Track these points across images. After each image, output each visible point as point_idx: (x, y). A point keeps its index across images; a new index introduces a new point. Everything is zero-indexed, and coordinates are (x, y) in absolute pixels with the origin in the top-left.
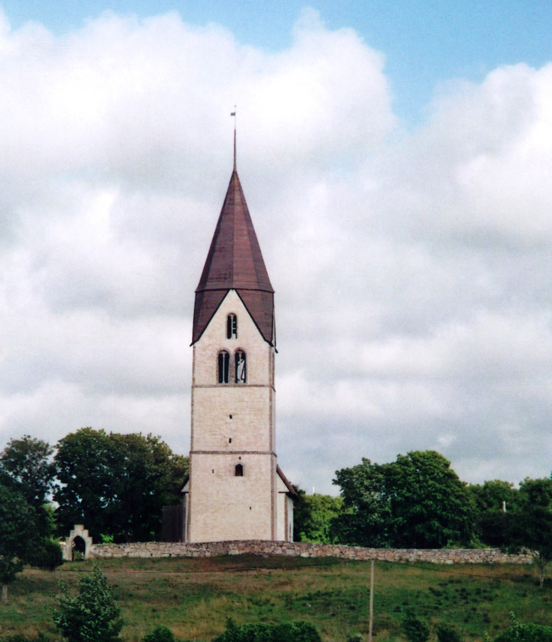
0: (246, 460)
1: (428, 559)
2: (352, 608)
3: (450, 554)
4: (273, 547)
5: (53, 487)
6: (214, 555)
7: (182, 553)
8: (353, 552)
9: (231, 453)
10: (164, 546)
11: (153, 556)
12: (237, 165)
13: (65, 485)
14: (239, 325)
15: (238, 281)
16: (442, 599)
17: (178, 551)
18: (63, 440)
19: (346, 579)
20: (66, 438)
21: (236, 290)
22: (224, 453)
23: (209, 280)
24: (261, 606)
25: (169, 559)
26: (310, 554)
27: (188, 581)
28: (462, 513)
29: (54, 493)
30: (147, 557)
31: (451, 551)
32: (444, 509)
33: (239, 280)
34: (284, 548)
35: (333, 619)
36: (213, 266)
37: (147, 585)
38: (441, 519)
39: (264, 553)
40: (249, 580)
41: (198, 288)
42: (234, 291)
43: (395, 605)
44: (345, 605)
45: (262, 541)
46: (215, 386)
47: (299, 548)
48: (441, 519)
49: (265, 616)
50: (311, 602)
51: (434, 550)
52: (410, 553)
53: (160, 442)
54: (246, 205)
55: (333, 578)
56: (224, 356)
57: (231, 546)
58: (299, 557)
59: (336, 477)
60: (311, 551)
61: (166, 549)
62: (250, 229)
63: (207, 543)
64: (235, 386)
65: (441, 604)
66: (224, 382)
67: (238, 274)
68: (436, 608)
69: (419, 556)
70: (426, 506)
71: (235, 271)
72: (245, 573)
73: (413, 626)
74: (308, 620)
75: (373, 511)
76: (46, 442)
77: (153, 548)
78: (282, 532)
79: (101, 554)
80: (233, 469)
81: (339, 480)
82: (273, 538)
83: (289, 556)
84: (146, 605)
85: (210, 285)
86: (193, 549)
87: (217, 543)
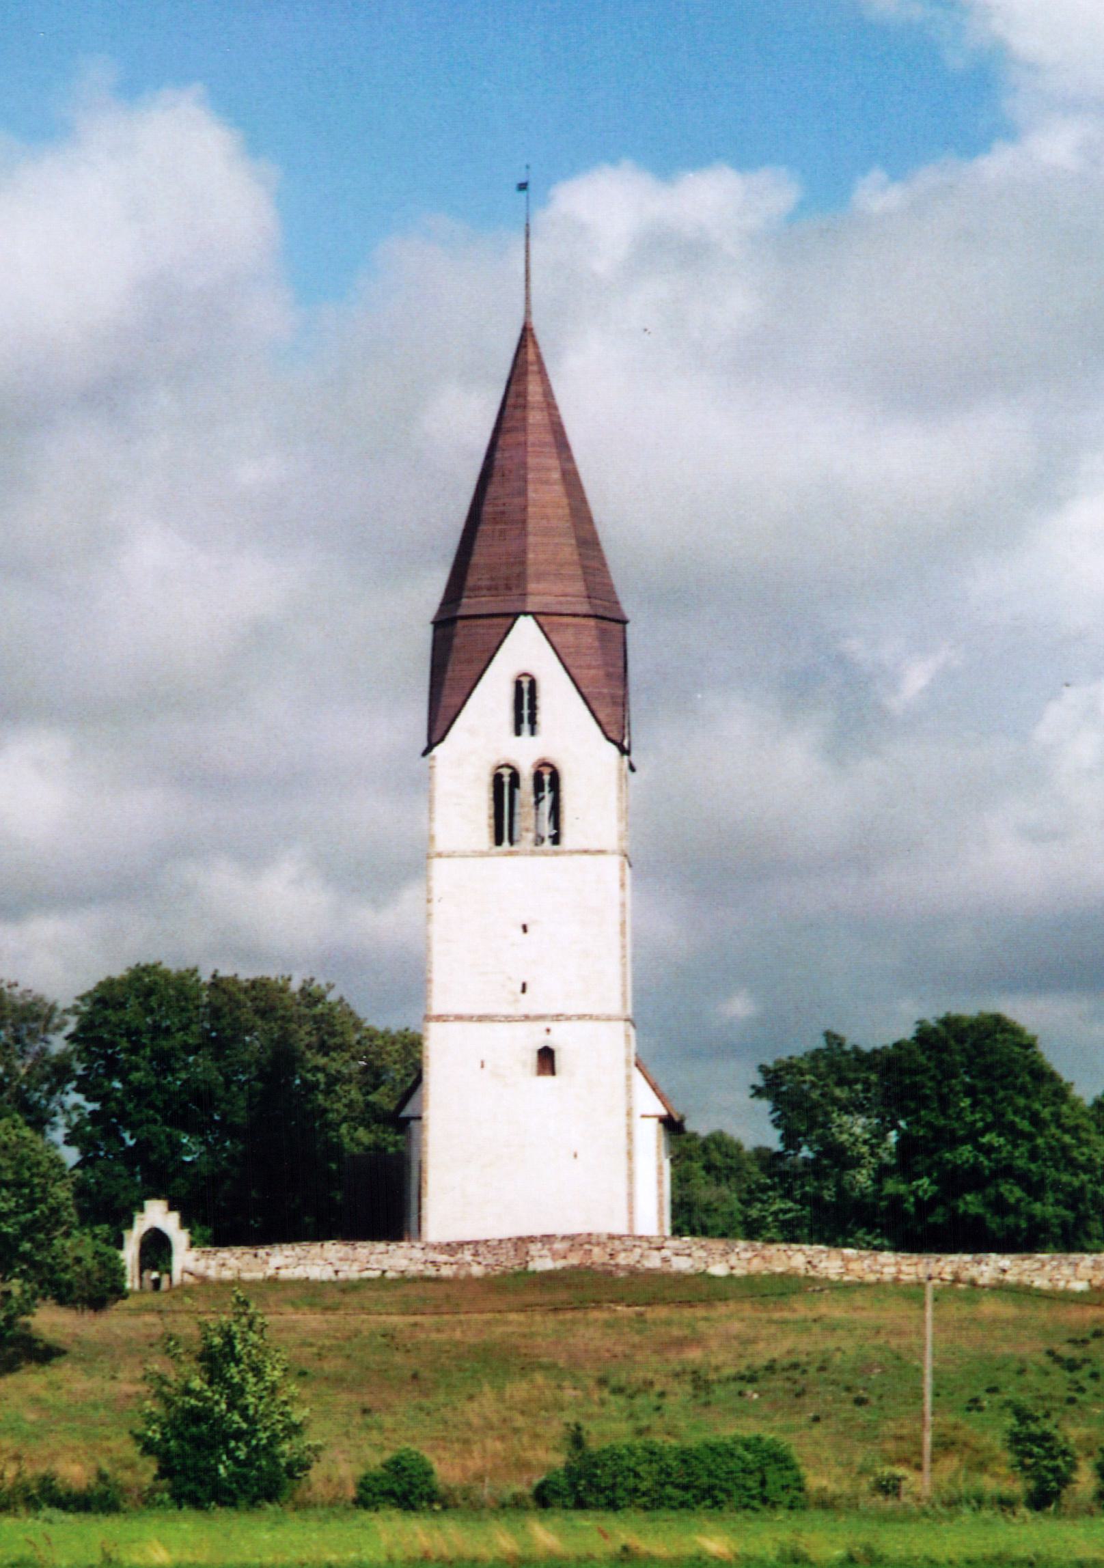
0: (560, 1037)
1: (1026, 1279)
2: (860, 1402)
3: (1082, 1265)
4: (638, 1251)
5: (66, 1112)
6: (493, 1273)
7: (414, 1269)
8: (839, 1263)
9: (527, 1018)
10: (366, 1251)
11: (341, 1275)
12: (534, 310)
13: (95, 1106)
14: (543, 701)
15: (539, 594)
16: (1084, 1378)
17: (402, 1264)
18: (89, 994)
19: (834, 1329)
20: (95, 991)
21: (534, 615)
22: (509, 1019)
23: (466, 593)
24: (631, 1397)
25: (382, 1282)
26: (732, 1268)
27: (443, 1337)
28: (1073, 1165)
29: (67, 1126)
30: (325, 1277)
31: (1083, 1259)
32: (1034, 1155)
33: (540, 594)
34: (665, 1253)
35: (818, 1430)
36: (478, 558)
37: (340, 1348)
38: (1022, 1179)
39: (617, 1265)
40: (591, 1332)
41: (436, 617)
42: (530, 618)
43: (967, 1394)
44: (844, 1394)
45: (611, 1237)
46: (482, 854)
47: (702, 1253)
48: (1022, 1179)
49: (644, 1423)
50: (755, 1386)
51: (1039, 1256)
52: (979, 1263)
53: (332, 997)
54: (555, 408)
55: (803, 1327)
56: (506, 779)
57: (534, 1249)
58: (705, 1276)
59: (760, 1082)
60: (733, 1260)
61: (373, 1257)
62: (568, 466)
63: (476, 1243)
64: (533, 853)
65: (1081, 1390)
66: (506, 843)
67: (540, 577)
68: (1071, 1401)
69: (1004, 1271)
70: (988, 1150)
71: (531, 570)
72: (579, 1315)
73: (1040, 1446)
74: (767, 1430)
75: (857, 1162)
76: (50, 999)
77: (341, 1255)
78: (650, 1212)
79: (212, 1273)
80: (533, 1058)
81: (768, 1086)
82: (631, 1227)
83: (679, 1273)
84: (344, 1397)
85: (468, 605)
86: (442, 1258)
87: (500, 1241)
